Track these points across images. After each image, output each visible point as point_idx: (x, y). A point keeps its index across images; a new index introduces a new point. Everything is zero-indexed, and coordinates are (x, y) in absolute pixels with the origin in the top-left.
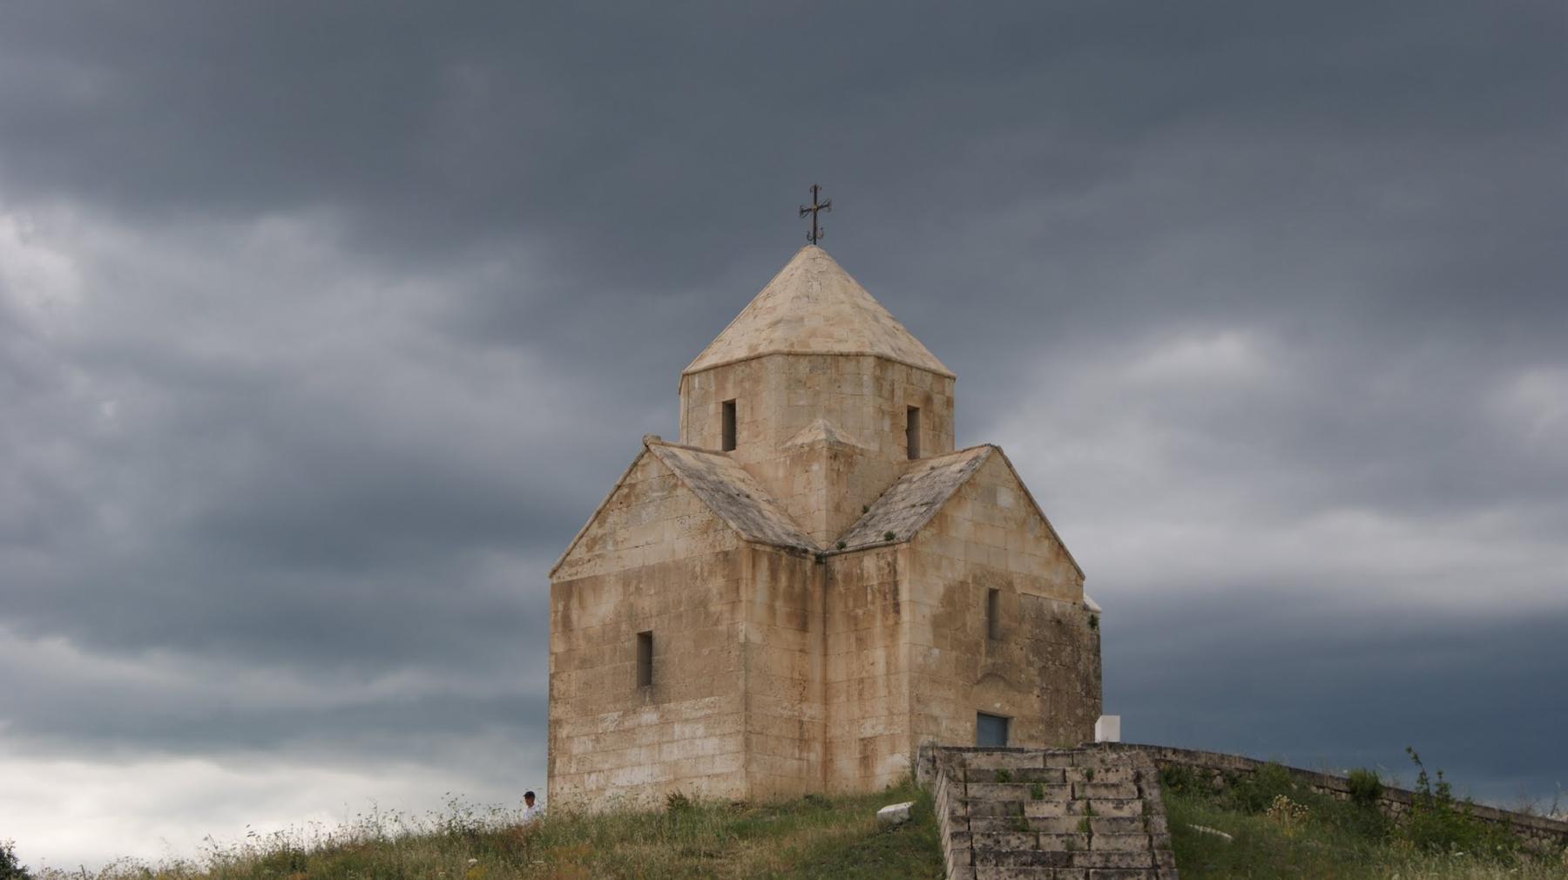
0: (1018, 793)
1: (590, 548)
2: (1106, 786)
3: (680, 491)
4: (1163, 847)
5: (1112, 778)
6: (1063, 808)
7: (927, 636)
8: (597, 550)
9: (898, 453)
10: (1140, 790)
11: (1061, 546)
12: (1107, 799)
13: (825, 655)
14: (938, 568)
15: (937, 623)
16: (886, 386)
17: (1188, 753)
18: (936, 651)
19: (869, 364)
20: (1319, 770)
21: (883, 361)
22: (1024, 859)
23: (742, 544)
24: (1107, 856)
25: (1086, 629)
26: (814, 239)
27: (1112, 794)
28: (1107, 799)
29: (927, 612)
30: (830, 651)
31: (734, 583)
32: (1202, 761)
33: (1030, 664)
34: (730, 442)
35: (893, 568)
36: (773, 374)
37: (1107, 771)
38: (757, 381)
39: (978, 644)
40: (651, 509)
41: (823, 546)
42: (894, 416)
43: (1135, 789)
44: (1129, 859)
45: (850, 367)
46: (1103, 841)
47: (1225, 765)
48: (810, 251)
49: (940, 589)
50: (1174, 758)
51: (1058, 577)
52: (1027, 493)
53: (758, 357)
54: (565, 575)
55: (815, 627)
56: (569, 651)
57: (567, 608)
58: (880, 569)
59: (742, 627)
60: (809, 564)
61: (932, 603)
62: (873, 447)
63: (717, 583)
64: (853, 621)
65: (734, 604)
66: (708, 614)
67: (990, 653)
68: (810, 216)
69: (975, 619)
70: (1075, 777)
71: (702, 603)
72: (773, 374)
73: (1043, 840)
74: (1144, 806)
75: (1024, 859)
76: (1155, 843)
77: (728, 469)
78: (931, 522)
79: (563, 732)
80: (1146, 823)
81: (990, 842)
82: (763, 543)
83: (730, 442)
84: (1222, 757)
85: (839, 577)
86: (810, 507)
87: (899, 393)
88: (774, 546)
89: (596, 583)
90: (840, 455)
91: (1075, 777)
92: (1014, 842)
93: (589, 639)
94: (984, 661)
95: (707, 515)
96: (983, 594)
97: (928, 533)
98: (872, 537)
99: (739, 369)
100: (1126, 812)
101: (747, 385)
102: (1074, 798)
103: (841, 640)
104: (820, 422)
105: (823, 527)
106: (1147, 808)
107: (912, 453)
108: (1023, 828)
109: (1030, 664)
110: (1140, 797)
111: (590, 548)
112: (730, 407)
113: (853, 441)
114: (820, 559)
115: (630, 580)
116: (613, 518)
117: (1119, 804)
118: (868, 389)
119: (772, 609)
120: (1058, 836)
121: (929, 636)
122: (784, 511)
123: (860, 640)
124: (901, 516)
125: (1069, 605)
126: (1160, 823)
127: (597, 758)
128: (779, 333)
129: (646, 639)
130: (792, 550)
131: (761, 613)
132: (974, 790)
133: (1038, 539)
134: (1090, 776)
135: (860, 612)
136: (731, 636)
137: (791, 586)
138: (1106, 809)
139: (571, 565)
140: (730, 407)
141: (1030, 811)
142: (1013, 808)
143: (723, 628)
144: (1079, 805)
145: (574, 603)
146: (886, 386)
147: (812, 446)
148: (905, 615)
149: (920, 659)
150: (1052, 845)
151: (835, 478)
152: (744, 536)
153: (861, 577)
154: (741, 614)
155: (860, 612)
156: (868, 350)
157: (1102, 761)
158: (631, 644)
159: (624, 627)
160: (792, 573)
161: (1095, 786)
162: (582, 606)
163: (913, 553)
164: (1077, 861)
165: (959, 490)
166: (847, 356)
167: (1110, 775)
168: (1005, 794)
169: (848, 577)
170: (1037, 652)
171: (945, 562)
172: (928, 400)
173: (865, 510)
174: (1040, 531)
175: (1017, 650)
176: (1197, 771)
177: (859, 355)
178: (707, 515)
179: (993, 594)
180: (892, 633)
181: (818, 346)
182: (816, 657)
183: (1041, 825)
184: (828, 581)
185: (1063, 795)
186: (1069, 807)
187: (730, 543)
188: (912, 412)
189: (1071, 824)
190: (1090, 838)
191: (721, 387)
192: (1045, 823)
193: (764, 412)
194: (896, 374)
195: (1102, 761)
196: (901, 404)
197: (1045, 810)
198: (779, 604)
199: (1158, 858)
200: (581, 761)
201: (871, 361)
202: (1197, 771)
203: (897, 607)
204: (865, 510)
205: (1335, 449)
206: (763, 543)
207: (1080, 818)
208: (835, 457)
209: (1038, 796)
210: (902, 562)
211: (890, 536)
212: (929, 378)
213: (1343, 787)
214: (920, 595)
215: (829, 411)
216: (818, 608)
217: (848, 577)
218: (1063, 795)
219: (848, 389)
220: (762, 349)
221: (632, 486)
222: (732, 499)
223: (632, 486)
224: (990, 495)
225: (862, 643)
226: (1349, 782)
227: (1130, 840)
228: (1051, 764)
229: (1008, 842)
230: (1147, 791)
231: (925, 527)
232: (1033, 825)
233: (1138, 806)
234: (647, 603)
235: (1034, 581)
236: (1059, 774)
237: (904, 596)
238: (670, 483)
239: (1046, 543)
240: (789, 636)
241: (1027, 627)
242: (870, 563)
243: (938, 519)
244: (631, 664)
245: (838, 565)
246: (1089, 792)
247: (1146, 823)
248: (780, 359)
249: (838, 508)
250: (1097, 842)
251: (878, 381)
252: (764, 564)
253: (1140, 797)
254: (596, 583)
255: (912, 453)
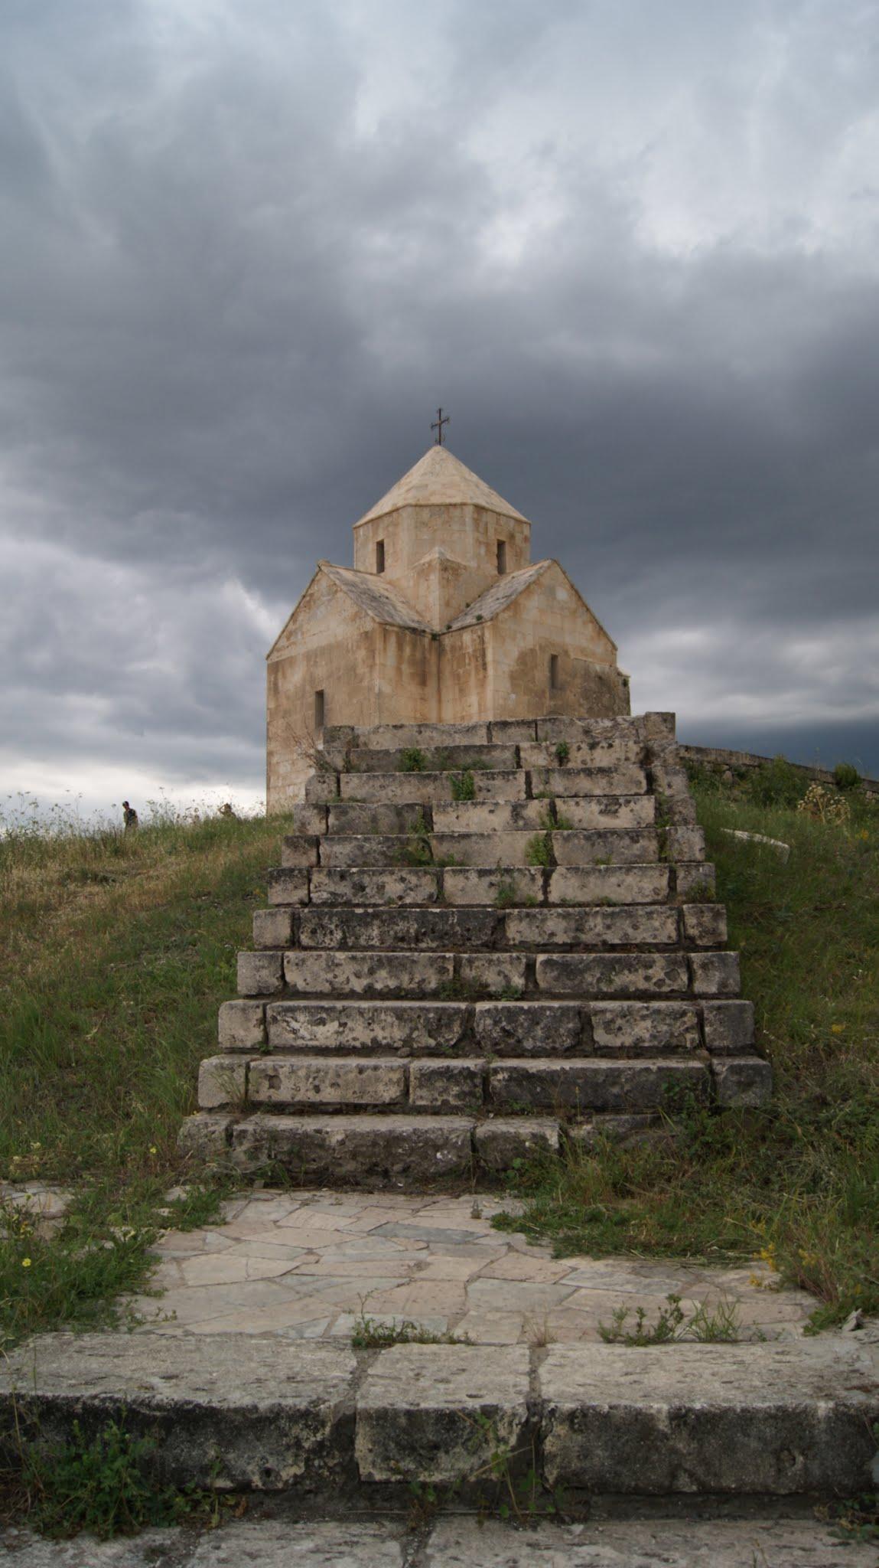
0: (430, 789)
1: (288, 639)
2: (589, 772)
3: (340, 595)
4: (699, 896)
5: (602, 758)
6: (504, 815)
7: (506, 684)
8: (293, 639)
9: (491, 569)
10: (651, 779)
11: (601, 628)
12: (588, 796)
13: (440, 701)
14: (514, 639)
15: (513, 677)
16: (482, 525)
17: (699, 750)
18: (513, 696)
19: (469, 510)
20: (810, 765)
21: (479, 509)
22: (401, 927)
23: (376, 626)
24: (577, 911)
25: (621, 687)
26: (440, 443)
27: (599, 787)
28: (588, 796)
29: (506, 669)
30: (443, 698)
31: (372, 652)
32: (712, 757)
33: (581, 705)
34: (381, 568)
35: (482, 641)
36: (406, 519)
37: (593, 746)
38: (396, 525)
39: (544, 692)
40: (323, 608)
41: (437, 628)
42: (487, 545)
43: (641, 776)
44: (626, 925)
45: (457, 512)
46: (574, 881)
47: (734, 761)
48: (438, 448)
49: (515, 654)
50: (687, 755)
51: (600, 648)
52: (576, 592)
53: (397, 510)
54: (275, 658)
55: (432, 683)
56: (278, 706)
57: (276, 679)
58: (473, 640)
59: (377, 682)
60: (427, 640)
61: (509, 663)
62: (473, 564)
63: (362, 653)
64: (458, 677)
65: (372, 667)
66: (356, 675)
67: (552, 698)
68: (437, 430)
69: (542, 675)
70: (536, 759)
71: (352, 668)
72: (406, 519)
73: (451, 882)
74: (658, 809)
75: (401, 927)
76: (681, 885)
77: (377, 584)
78: (508, 608)
79: (275, 760)
80: (663, 841)
81: (344, 889)
82: (392, 625)
83: (381, 568)
84: (731, 754)
85: (448, 648)
86: (425, 601)
87: (491, 531)
88: (400, 627)
89: (291, 661)
90: (448, 568)
91: (536, 759)
92: (394, 888)
93: (288, 698)
94: (548, 703)
95: (356, 609)
96: (547, 658)
97: (506, 615)
98: (470, 620)
99: (386, 520)
100: (624, 820)
101: (390, 529)
102: (530, 796)
103: (449, 692)
104: (437, 549)
105: (437, 616)
106: (664, 812)
107: (501, 570)
108: (418, 861)
109: (581, 705)
110: (650, 791)
111: (288, 639)
112: (381, 545)
113: (459, 560)
114: (435, 637)
115: (311, 657)
116: (301, 617)
117: (611, 804)
118: (469, 527)
119: (399, 670)
120: (482, 873)
121: (508, 685)
122: (412, 608)
123: (461, 690)
124: (488, 607)
125: (607, 668)
126: (690, 841)
127: (293, 776)
128: (410, 495)
129: (320, 695)
130: (414, 630)
131: (391, 672)
132: (353, 786)
133: (584, 623)
134: (562, 756)
135: (461, 671)
136: (370, 689)
137: (413, 655)
138: (587, 814)
139: (278, 650)
140: (381, 545)
141: (442, 822)
142: (410, 818)
143: (365, 683)
144: (535, 810)
145: (280, 675)
146: (482, 525)
147: (430, 563)
148: (490, 671)
149: (501, 702)
150: (469, 890)
151: (445, 583)
152: (377, 619)
153: (461, 648)
154: (376, 674)
155: (461, 671)
156: (469, 501)
157: (587, 732)
158: (311, 699)
159: (308, 688)
160: (414, 646)
161: (568, 773)
162: (284, 677)
163: (495, 628)
164: (516, 930)
165: (528, 587)
166: (455, 505)
167: (598, 752)
168: (407, 791)
169: (453, 648)
170: (587, 698)
171: (519, 636)
172: (512, 536)
173: (468, 605)
174: (586, 617)
175: (571, 696)
176: (708, 767)
177: (463, 504)
178: (356, 609)
179: (554, 658)
180: (482, 683)
181: (436, 500)
182: (433, 703)
183: (455, 850)
184: (441, 652)
185: (512, 790)
186: (517, 811)
187: (369, 626)
188: (501, 545)
189: (512, 848)
190: (547, 876)
191: (375, 533)
192: (464, 845)
193: (400, 547)
194: (487, 518)
195: (587, 732)
196: (493, 538)
197: (473, 818)
198: (405, 667)
199: (691, 920)
200: (284, 778)
201: (471, 508)
202: (708, 767)
203: (484, 666)
204: (468, 605)
205: (723, 669)
206: (392, 625)
207: (531, 835)
208: (445, 569)
209: (466, 794)
210: (488, 635)
211: (479, 618)
212: (512, 523)
213: (830, 780)
214: (501, 658)
215: (443, 542)
216: (434, 669)
217: (453, 648)
218: (512, 790)
219: (456, 527)
220: (400, 504)
221: (312, 595)
222: (374, 598)
223: (312, 595)
224: (551, 592)
225: (462, 691)
226: (835, 775)
227: (630, 879)
228: (498, 738)
229: (381, 888)
230: (663, 780)
231: (504, 611)
232: (440, 850)
233: (646, 808)
234: (321, 671)
235: (583, 651)
236: (508, 755)
237: (489, 657)
238: (333, 590)
239: (590, 626)
240: (413, 688)
241: (578, 681)
242: (467, 637)
243: (513, 605)
244: (311, 713)
245: (447, 641)
246: (558, 784)
247: (663, 841)
248: (409, 509)
249: (448, 604)
250: (562, 886)
251: (476, 522)
252: (393, 640)
253: (650, 791)
254: (291, 661)
255: (501, 570)
